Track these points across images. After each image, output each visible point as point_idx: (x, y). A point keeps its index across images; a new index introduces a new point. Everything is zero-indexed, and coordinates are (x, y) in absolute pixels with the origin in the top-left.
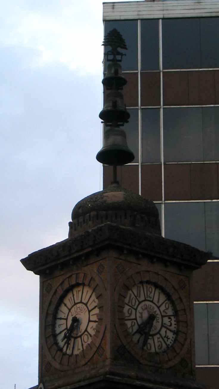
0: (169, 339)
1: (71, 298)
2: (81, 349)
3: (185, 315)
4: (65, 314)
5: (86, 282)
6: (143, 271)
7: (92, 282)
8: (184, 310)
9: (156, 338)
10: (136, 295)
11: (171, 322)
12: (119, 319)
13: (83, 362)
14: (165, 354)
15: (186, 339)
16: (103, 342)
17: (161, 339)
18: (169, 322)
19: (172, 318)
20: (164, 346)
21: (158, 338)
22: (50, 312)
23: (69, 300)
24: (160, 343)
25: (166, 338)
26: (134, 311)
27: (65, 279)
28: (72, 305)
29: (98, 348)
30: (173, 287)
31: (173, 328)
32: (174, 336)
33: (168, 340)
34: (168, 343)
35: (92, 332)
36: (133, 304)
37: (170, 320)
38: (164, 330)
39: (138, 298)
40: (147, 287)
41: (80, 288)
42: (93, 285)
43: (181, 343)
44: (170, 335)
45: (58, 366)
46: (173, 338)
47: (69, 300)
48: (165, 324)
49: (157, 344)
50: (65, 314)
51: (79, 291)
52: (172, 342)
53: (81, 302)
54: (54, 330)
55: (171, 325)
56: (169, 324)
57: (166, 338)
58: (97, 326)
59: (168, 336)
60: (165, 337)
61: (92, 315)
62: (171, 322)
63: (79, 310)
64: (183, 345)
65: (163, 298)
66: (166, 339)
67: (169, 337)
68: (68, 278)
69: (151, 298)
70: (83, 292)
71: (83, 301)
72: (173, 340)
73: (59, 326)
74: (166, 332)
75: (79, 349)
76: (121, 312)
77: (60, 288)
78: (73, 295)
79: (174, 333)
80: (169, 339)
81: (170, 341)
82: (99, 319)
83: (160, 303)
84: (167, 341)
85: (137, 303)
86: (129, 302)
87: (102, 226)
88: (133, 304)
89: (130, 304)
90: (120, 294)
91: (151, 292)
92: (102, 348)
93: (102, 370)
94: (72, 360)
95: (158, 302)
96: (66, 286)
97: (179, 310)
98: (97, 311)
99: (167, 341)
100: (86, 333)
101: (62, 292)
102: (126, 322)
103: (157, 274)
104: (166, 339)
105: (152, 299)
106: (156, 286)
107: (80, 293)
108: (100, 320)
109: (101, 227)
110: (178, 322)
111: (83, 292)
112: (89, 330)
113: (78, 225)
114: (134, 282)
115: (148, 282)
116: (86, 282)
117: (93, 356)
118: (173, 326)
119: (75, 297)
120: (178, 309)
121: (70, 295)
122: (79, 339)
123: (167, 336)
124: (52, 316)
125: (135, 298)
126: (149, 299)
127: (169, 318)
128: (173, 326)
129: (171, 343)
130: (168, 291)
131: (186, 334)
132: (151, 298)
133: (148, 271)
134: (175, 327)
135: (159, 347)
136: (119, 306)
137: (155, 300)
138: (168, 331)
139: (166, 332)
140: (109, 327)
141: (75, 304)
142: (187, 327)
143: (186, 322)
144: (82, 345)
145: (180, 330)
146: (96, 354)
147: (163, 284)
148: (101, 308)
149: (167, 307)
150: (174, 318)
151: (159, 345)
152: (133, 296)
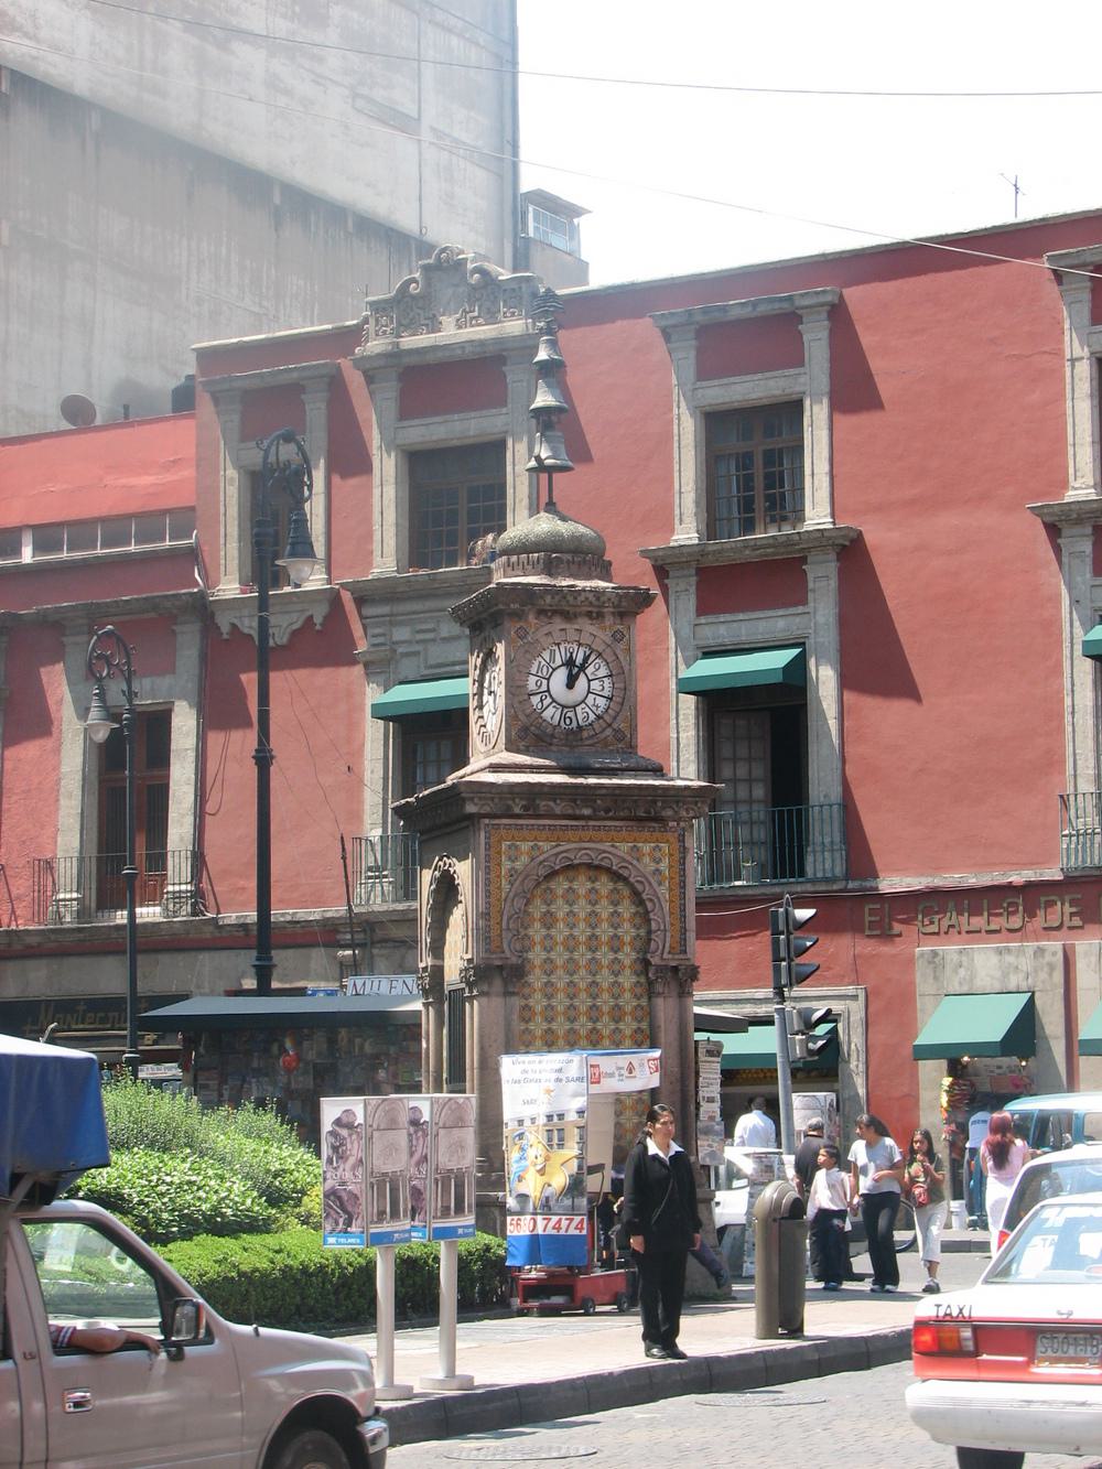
85: (551, 670)
152: (543, 663)
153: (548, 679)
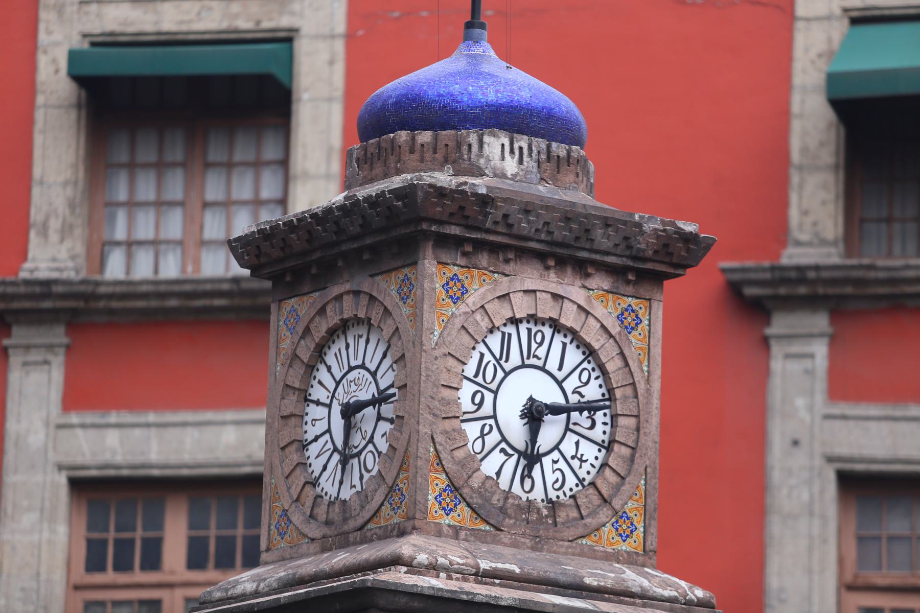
2: (359, 488)
9: (547, 461)
10: (498, 357)
17: (562, 464)
20: (571, 481)
23: (336, 354)
24: (558, 474)
26: (489, 397)
27: (327, 303)
28: (344, 372)
34: (582, 474)
35: (383, 446)
36: (489, 379)
39: (502, 362)
40: (529, 330)
41: (363, 331)
44: (590, 451)
46: (596, 458)
47: (336, 354)
48: (575, 424)
49: (550, 478)
51: (360, 336)
53: (363, 366)
59: (582, 455)
60: (573, 457)
63: (354, 387)
65: (574, 356)
66: (575, 463)
69: (539, 359)
71: (368, 365)
72: (597, 464)
74: (577, 443)
75: (354, 486)
79: (600, 445)
81: (587, 467)
83: (567, 367)
84: (581, 467)
85: (500, 374)
86: (476, 375)
88: (489, 379)
91: (540, 344)
93: (474, 182)
99: (581, 467)
102: (465, 426)
104: (575, 463)
105: (540, 363)
111: (367, 342)
112: (377, 439)
118: (599, 428)
122: (355, 461)
123: (579, 456)
125: (493, 361)
126: (533, 361)
129: (588, 473)
130: (588, 341)
132: (539, 359)
134: (604, 433)
135: (557, 486)
137: (552, 365)
139: (577, 443)
141: (351, 369)
144: (361, 477)
149: (584, 379)
151: (557, 480)
152: (488, 357)
153: (496, 393)
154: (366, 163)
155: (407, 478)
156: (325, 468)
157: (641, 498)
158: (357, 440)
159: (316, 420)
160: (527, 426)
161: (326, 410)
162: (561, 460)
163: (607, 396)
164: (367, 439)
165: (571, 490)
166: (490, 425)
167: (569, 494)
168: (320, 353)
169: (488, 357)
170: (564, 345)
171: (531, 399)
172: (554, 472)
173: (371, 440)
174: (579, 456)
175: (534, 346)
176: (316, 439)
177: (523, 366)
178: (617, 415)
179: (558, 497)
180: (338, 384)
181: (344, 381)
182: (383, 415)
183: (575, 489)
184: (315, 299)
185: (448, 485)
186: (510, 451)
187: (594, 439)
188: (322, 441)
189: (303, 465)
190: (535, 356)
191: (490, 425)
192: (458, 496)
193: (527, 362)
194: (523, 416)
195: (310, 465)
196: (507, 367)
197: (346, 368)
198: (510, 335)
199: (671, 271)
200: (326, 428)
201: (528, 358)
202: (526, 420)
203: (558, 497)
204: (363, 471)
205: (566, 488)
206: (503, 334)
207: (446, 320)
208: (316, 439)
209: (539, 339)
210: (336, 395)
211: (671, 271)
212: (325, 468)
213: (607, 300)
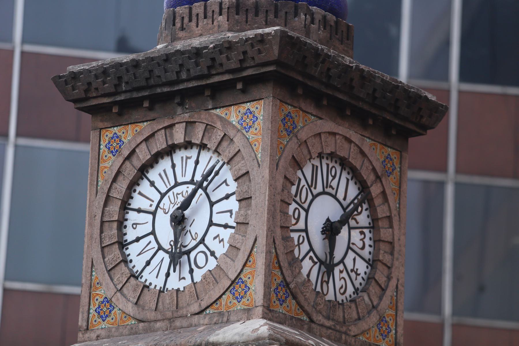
0: (359, 274)
1: (165, 171)
3: (390, 230)
4: (153, 201)
5: (212, 145)
6: (325, 132)
7: (225, 144)
8: (389, 218)
11: (364, 240)
12: (282, 227)
13: (195, 308)
14: (353, 305)
15: (389, 278)
16: (247, 270)
17: (345, 275)
18: (361, 240)
19: (366, 231)
21: (341, 272)
22: (114, 194)
25: (353, 273)
26: (303, 213)
29: (233, 282)
30: (374, 169)
31: (366, 253)
32: (368, 271)
33: (358, 277)
36: (303, 200)
37: (363, 236)
38: (351, 255)
39: (312, 189)
40: (328, 165)
41: (193, 153)
42: (228, 151)
43: (380, 286)
45: (130, 308)
46: (365, 273)
48: (353, 244)
50: (153, 201)
51: (188, 158)
52: (363, 283)
54: (121, 234)
55: (363, 248)
56: (360, 245)
57: (353, 273)
58: (232, 237)
59: (357, 269)
60: (352, 271)
61: (217, 213)
62: (364, 240)
64: (384, 290)
66: (353, 275)
67: (358, 272)
68: (165, 128)
69: (333, 189)
70: (197, 162)
72: (365, 277)
73: (134, 226)
74: (354, 260)
76: (285, 213)
77: (144, 146)
78: (173, 166)
80: (359, 274)
81: (359, 278)
82: (237, 223)
84: (356, 279)
85: (310, 197)
86: (296, 196)
87: (269, 34)
88: (303, 200)
89: (297, 199)
90: (286, 177)
91: (334, 177)
92: (243, 282)
94: (166, 299)
95: (345, 199)
96: (160, 143)
97: (381, 218)
98: (233, 204)
99: (356, 279)
100: (201, 247)
101: (149, 157)
103: (349, 141)
104: (353, 275)
106: (344, 163)
107: (191, 163)
108: (242, 224)
109: (262, 35)
110: (377, 241)
111: (197, 162)
113: (190, 20)
114: (310, 153)
115: (332, 156)
116: (212, 145)
117: (220, 297)
118: (367, 249)
119: (178, 169)
120: (380, 216)
121: (165, 164)
124: (119, 202)
125: (306, 186)
127: (362, 233)
128: (367, 249)
129: (361, 284)
131: (389, 268)
133: (334, 134)
134: (370, 253)
135: (342, 291)
136: (282, 201)
137: (340, 195)
138: (358, 259)
139: (354, 260)
140: (262, 242)
141: (177, 184)
142: (392, 254)
143: (391, 243)
145: (381, 258)
146: (228, 293)
147: (356, 161)
148: (244, 200)
150: (370, 232)
151: (342, 287)
152: (303, 182)
153: (307, 211)
154: (220, 14)
155: (250, 273)
156: (148, 263)
157: (393, 306)
158: (189, 242)
159: (136, 224)
160: (327, 240)
161: (151, 217)
162: (345, 271)
163: (372, 225)
164: (198, 239)
165: (350, 296)
166: (303, 237)
167: (349, 299)
168: (143, 171)
169: (303, 182)
170: (348, 180)
171: (328, 220)
172: (340, 280)
173: (202, 241)
174: (355, 270)
175: (330, 178)
176: (138, 240)
177: (324, 193)
178: (380, 241)
179: (343, 301)
180: (163, 196)
181: (170, 194)
182: (214, 222)
183: (353, 296)
184: (145, 128)
185: (282, 281)
186: (315, 260)
187: (363, 256)
188: (143, 242)
189: (125, 261)
190: (331, 187)
191: (303, 237)
192: (288, 291)
193: (326, 190)
194: (323, 232)
195: (131, 261)
196: (315, 192)
197: (173, 183)
198: (317, 167)
199: (418, 130)
200: (150, 230)
201: (327, 187)
202: (324, 236)
203: (343, 301)
204: (193, 266)
205: (347, 294)
206: (313, 165)
207: (283, 147)
208: (138, 240)
209: (333, 174)
210: (161, 205)
211: (418, 130)
212: (148, 263)
213: (377, 148)
